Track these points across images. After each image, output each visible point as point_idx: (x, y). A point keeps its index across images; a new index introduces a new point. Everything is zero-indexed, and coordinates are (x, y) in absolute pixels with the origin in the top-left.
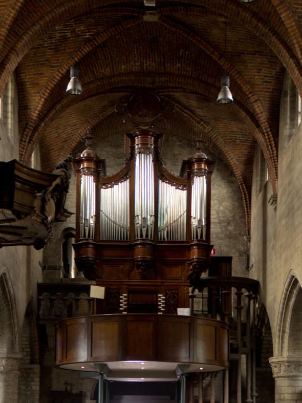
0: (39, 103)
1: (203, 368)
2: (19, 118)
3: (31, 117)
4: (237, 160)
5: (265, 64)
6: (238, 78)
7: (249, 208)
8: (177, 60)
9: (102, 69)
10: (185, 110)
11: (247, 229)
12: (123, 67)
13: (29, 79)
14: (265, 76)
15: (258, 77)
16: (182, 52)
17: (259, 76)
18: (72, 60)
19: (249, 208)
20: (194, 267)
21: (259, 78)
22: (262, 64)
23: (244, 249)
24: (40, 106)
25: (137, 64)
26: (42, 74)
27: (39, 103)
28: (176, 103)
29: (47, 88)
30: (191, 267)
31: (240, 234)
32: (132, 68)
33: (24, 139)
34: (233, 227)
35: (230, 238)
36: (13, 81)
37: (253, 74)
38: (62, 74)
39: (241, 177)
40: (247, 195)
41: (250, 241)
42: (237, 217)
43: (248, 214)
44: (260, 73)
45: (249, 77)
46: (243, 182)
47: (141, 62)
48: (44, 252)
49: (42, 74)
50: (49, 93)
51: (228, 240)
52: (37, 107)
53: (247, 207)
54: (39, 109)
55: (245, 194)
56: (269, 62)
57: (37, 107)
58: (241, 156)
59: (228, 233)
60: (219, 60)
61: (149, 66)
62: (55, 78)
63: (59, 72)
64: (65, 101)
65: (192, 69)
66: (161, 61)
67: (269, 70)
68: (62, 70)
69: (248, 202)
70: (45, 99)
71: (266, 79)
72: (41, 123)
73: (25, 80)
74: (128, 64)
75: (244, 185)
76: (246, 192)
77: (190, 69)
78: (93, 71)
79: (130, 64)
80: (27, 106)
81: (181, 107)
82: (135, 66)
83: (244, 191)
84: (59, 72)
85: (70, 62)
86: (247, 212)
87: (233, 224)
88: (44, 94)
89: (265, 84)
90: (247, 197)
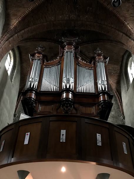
0: (15, 22)
1: (61, 173)
2: (3, 28)
3: (10, 28)
4: (113, 82)
5: (131, 7)
6: (118, 14)
7: (121, 103)
8: (86, 14)
9: (50, 17)
10: (88, 59)
11: (122, 113)
12: (61, 17)
13: (12, 12)
14: (132, 14)
15: (127, 14)
16: (89, 8)
17: (128, 13)
18: (35, 4)
19: (121, 103)
20: (102, 106)
21: (128, 15)
22: (129, 7)
23: (122, 123)
24: (16, 24)
25: (67, 16)
26: (19, 11)
27: (15, 22)
28: (84, 55)
29: (21, 16)
30: (100, 107)
31: (118, 116)
32: (65, 18)
33: (3, 37)
34: (114, 113)
35: (113, 117)
36: (3, 7)
37: (125, 12)
38: (29, 11)
39: (115, 89)
40: (119, 97)
41: (124, 119)
42: (116, 108)
43: (121, 106)
44: (128, 12)
45: (123, 14)
46: (116, 91)
47: (69, 15)
48: (19, 119)
49: (19, 11)
50: (21, 19)
51: (112, 119)
52: (14, 24)
53: (120, 103)
54: (15, 25)
55: (118, 97)
56: (133, 6)
57: (14, 24)
58: (114, 80)
59: (112, 115)
60: (108, 5)
61: (73, 17)
62: (25, 12)
63: (28, 9)
64: (30, 28)
65: (93, 18)
66: (78, 14)
67: (133, 10)
68: (29, 9)
69: (121, 101)
70: (19, 21)
71: (132, 15)
72: (15, 34)
73: (10, 13)
74: (63, 16)
75: (117, 93)
76: (119, 96)
77: (92, 18)
78: (46, 17)
79: (64, 15)
80: (9, 24)
81: (86, 57)
82: (66, 17)
83: (117, 96)
84: (28, 9)
85: (34, 5)
86: (121, 105)
87: (114, 111)
88: (18, 19)
89: (131, 17)
90: (120, 98)
